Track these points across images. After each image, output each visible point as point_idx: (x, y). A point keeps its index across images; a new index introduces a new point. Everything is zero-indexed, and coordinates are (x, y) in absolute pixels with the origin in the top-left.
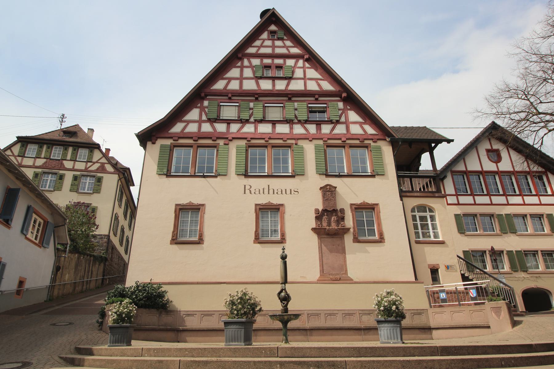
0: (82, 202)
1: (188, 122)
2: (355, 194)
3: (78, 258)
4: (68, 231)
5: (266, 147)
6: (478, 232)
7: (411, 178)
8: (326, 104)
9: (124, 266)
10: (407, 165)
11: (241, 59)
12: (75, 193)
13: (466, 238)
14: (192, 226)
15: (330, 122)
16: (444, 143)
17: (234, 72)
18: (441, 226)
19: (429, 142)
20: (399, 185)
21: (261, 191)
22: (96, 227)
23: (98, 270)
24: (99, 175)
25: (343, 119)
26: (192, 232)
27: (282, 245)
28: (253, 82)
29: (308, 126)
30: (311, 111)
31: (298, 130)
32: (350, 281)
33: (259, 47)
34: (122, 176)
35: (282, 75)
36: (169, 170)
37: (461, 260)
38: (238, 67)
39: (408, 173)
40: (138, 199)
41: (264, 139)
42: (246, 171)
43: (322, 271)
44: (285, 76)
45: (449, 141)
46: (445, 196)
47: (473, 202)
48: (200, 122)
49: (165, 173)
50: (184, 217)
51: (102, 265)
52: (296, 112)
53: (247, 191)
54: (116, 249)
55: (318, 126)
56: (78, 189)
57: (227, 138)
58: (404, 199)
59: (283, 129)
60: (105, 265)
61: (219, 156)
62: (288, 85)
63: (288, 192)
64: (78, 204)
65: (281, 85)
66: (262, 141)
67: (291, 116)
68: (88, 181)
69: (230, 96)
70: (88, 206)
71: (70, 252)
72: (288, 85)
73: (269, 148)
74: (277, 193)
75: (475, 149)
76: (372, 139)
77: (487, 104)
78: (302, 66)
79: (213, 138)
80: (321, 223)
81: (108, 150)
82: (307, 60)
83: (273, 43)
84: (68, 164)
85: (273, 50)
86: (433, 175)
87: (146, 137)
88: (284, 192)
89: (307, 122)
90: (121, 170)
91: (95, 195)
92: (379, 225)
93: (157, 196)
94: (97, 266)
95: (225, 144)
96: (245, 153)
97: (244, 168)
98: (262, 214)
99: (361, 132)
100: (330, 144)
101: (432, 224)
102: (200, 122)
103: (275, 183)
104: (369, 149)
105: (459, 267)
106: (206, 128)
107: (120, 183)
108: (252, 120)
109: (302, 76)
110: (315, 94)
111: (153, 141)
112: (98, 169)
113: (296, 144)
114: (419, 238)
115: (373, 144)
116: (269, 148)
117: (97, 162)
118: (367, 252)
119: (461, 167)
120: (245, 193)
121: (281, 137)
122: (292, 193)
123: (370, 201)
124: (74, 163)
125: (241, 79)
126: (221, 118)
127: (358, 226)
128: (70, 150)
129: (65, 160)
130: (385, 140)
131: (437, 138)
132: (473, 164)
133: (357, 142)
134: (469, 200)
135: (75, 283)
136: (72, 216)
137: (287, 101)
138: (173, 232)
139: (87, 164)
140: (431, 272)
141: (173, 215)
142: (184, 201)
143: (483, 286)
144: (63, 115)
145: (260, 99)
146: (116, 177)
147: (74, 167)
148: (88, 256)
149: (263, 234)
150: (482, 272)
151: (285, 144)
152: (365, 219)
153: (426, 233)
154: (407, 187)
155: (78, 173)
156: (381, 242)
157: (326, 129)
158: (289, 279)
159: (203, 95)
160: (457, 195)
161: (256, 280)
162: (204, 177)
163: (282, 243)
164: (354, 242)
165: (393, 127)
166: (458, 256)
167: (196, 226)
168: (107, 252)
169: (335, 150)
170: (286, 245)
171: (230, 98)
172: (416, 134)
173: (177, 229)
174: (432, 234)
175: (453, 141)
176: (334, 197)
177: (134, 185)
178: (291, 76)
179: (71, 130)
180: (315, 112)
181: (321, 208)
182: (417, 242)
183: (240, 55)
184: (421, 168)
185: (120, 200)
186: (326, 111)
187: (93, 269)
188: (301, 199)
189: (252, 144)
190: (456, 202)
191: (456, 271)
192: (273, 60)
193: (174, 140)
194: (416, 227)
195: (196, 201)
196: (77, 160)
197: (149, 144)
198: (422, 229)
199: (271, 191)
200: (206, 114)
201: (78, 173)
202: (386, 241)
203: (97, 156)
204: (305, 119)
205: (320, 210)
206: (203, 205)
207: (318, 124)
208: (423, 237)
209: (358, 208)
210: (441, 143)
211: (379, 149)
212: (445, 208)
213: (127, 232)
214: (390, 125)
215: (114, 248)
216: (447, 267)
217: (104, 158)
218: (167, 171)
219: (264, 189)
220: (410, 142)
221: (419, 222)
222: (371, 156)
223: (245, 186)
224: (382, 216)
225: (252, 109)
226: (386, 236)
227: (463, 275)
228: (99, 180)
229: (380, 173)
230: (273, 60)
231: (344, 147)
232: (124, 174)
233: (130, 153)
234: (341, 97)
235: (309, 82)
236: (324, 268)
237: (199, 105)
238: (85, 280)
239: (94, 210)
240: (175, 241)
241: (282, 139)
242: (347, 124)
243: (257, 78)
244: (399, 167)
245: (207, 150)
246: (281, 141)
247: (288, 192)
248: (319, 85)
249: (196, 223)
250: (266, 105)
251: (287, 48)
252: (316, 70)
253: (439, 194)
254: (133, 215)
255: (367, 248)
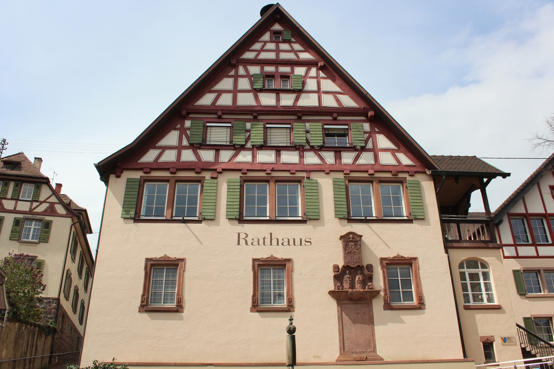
0: (25, 254)
1: (164, 148)
2: (386, 244)
3: (19, 329)
4: (7, 293)
5: (268, 181)
6: (542, 293)
7: (458, 223)
8: (347, 125)
9: (79, 340)
10: (453, 207)
11: (235, 67)
12: (16, 242)
13: (527, 301)
14: (168, 287)
15: (353, 148)
16: (499, 178)
17: (226, 83)
18: (496, 286)
19: (480, 176)
20: (444, 232)
21: (261, 242)
22: (42, 288)
23: (44, 344)
24: (47, 218)
25: (370, 145)
26: (167, 295)
27: (289, 314)
28: (251, 96)
29: (324, 154)
30: (328, 134)
31: (311, 159)
32: (380, 361)
33: (259, 52)
34: (76, 220)
35: (289, 88)
36: (138, 213)
37: (522, 330)
38: (231, 76)
39: (454, 217)
40: (97, 251)
41: (265, 171)
42: (241, 213)
43: (343, 348)
44: (293, 88)
45: (505, 175)
46: (501, 247)
47: (535, 255)
48: (180, 148)
49: (133, 216)
50: (157, 276)
51: (50, 338)
52: (308, 135)
53: (242, 242)
54: (68, 317)
55: (338, 153)
56: (20, 237)
57: (216, 170)
58: (449, 250)
59: (290, 158)
60: (53, 338)
61: (204, 194)
62: (297, 99)
63: (298, 242)
64: (19, 258)
65: (287, 100)
66: (263, 174)
67: (301, 140)
68: (33, 226)
69: (219, 114)
70: (33, 259)
71: (9, 320)
72: (297, 99)
73: (272, 184)
74: (282, 244)
75: (536, 186)
76: (408, 172)
77: (550, 128)
78: (315, 75)
79: (196, 170)
80: (342, 285)
81: (59, 186)
82: (322, 68)
83: (278, 47)
84: (8, 204)
85: (277, 55)
86: (485, 219)
87: (108, 169)
88: (291, 242)
89: (323, 148)
90: (76, 212)
91: (42, 245)
92: (418, 286)
93: (123, 248)
94: (43, 339)
95: (212, 178)
96: (239, 190)
97: (238, 210)
98: (262, 273)
99: (393, 162)
100: (352, 178)
101: (485, 284)
102: (180, 148)
103: (281, 231)
104: (405, 185)
105: (519, 339)
106: (188, 156)
107: (73, 229)
108: (249, 145)
109: (315, 88)
110: (218, 110)
111: (118, 174)
112: (46, 211)
113: (308, 178)
114: (469, 302)
115: (409, 178)
116: (272, 184)
117: (45, 202)
118: (402, 322)
119: (520, 209)
120: (239, 244)
121: (287, 167)
122: (303, 244)
123: (407, 254)
124: (16, 203)
125: (235, 91)
126: (208, 143)
127: (390, 288)
128: (12, 185)
129: (5, 199)
130: (425, 173)
131: (489, 171)
132: (535, 206)
133: (389, 175)
134: (530, 251)
135: (15, 361)
136: (12, 272)
137: (295, 121)
138: (143, 296)
139: (32, 204)
140: (484, 346)
141: (143, 273)
142: (157, 254)
143: (549, 363)
144: (4, 141)
145: (260, 117)
146: (68, 222)
147: (15, 208)
148: (31, 326)
149: (263, 300)
150: (547, 345)
151: (294, 178)
152: (399, 278)
153: (478, 295)
154: (453, 235)
155: (21, 216)
156: (420, 308)
157: (347, 158)
158: (299, 359)
159: (184, 112)
160: (515, 245)
161: (254, 361)
162: (184, 221)
163: (289, 311)
164: (385, 309)
165: (435, 156)
166: (518, 325)
167: (173, 288)
168: (56, 321)
169: (360, 186)
170: (297, 314)
171: (220, 117)
172: (464, 166)
173: (148, 292)
174: (485, 297)
175: (509, 175)
176: (360, 249)
177: (91, 232)
178: (301, 88)
179: (14, 159)
180: (333, 135)
181: (341, 264)
182: (467, 308)
183: (234, 62)
184: (471, 210)
185: (74, 253)
186: (348, 134)
187: (39, 344)
188: (314, 253)
189: (249, 178)
190: (515, 255)
191: (516, 344)
192: (277, 68)
193: (145, 173)
194: (465, 288)
195: (173, 254)
196: (20, 198)
197: (112, 178)
198: (472, 291)
199: (274, 242)
200: (188, 138)
201: (21, 216)
202: (426, 307)
203: (45, 193)
204: (319, 144)
205: (341, 267)
206: (182, 260)
207: (338, 151)
208: (474, 300)
209: (390, 264)
210: (495, 177)
211: (418, 185)
212: (502, 262)
213: (82, 295)
214: (430, 154)
215: (65, 315)
216: (504, 340)
217: (54, 197)
218: (135, 212)
219: (264, 238)
220: (457, 176)
221: (468, 282)
222: (407, 194)
223: (239, 234)
224: (422, 273)
225: (249, 131)
226: (427, 300)
227: (523, 350)
228: (48, 225)
229: (418, 217)
230: (277, 68)
231: (371, 182)
232: (79, 218)
233: (88, 191)
234: (366, 116)
235: (324, 96)
236: (346, 345)
237: (179, 126)
238: (28, 357)
239: (40, 265)
240: (145, 308)
241: (289, 171)
242: (375, 151)
243: (256, 91)
244: (443, 210)
245: (188, 186)
246: (287, 174)
247: (298, 242)
248: (338, 100)
249: (172, 284)
250: (267, 126)
251: (296, 52)
252: (334, 81)
253: (493, 244)
254: (90, 273)
255: (401, 317)
